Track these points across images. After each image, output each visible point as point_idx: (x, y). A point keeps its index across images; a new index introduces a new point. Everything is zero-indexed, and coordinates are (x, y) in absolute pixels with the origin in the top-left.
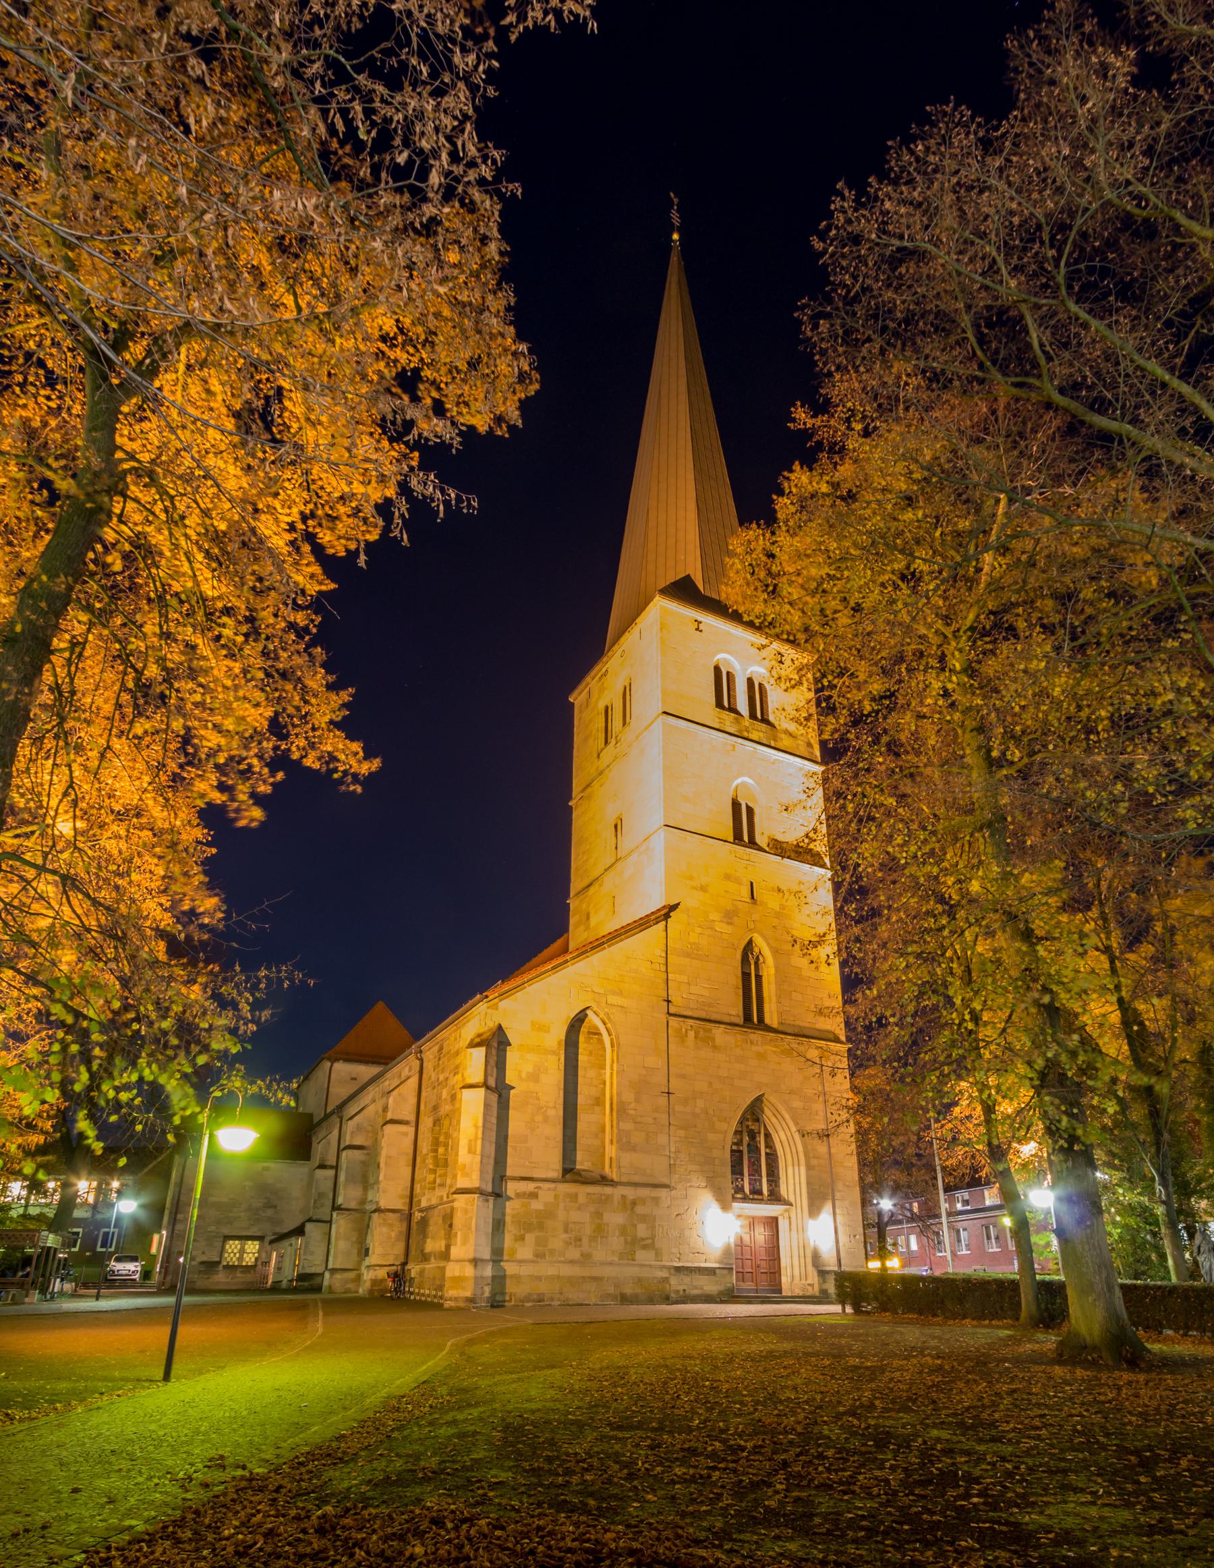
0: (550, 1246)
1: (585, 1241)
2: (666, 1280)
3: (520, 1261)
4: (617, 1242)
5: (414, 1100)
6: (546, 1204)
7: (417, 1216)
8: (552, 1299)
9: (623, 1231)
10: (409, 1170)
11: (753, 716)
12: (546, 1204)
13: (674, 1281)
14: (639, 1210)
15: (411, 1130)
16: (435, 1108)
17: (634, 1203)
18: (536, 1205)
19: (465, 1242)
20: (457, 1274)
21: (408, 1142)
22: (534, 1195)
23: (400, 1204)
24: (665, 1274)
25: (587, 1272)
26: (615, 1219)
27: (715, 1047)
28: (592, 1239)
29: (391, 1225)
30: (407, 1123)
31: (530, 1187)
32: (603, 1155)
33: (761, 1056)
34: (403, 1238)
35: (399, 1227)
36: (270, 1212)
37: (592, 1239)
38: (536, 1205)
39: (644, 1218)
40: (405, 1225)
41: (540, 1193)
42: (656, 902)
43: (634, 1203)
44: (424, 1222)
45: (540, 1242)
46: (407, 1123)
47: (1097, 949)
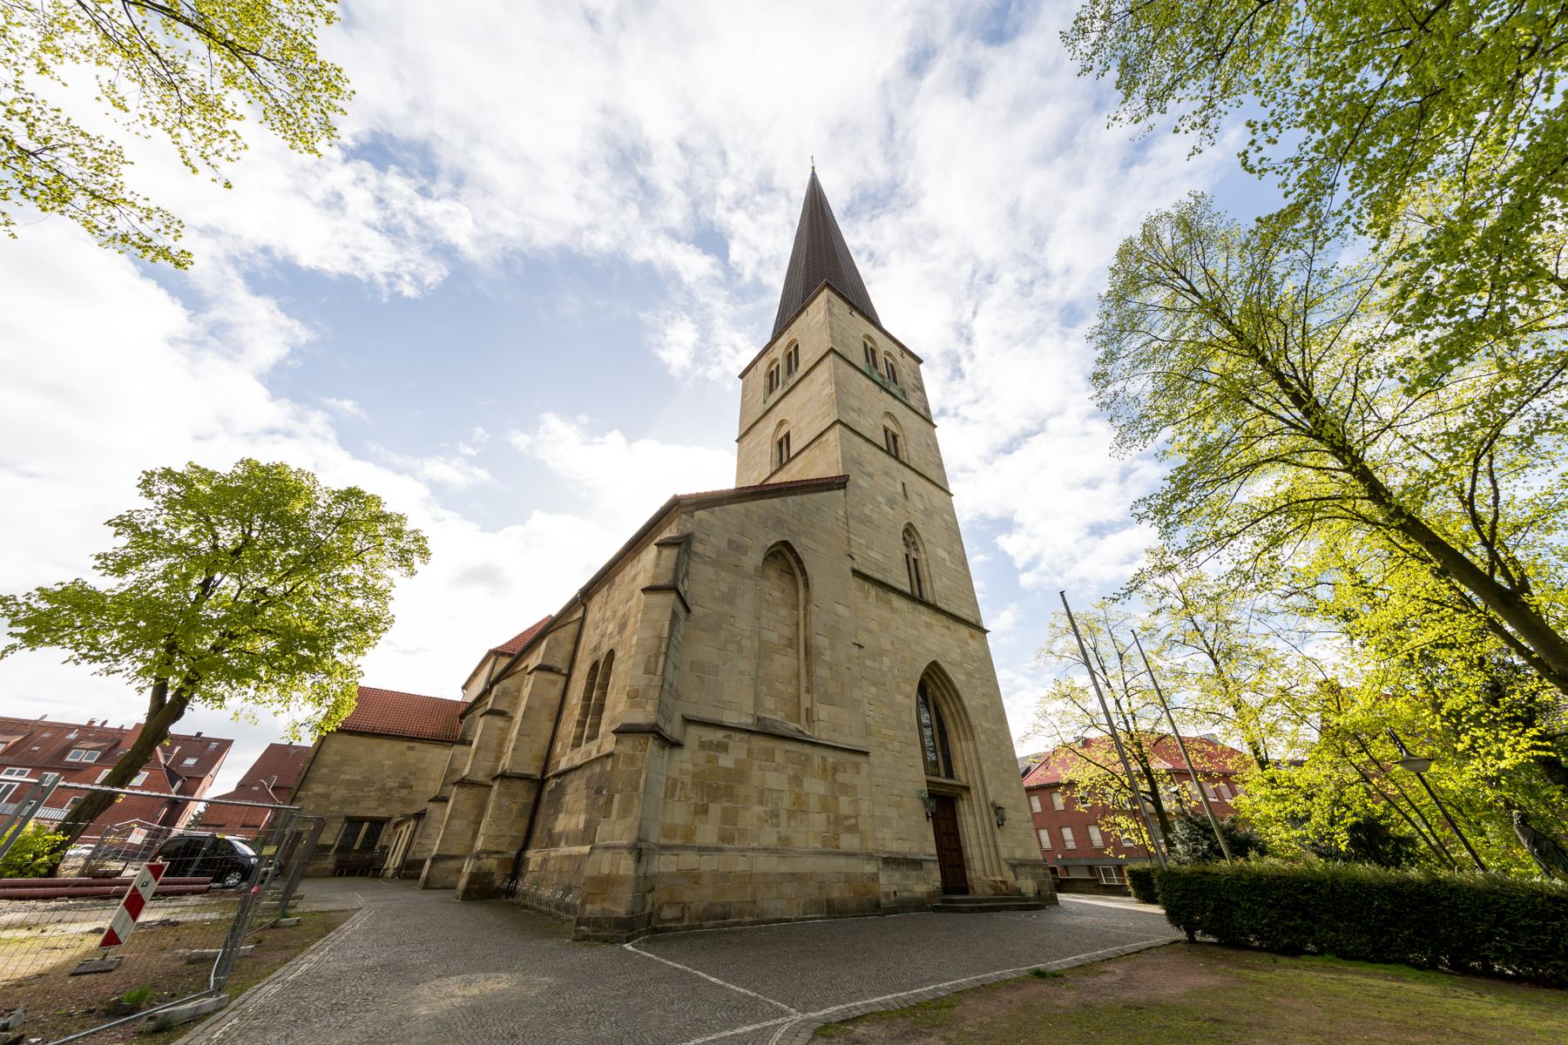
0: (741, 824)
1: (783, 816)
3: (702, 850)
4: (818, 821)
5: (570, 647)
6: (737, 762)
8: (741, 913)
10: (551, 725)
12: (737, 762)
13: (883, 879)
14: (841, 777)
15: (561, 681)
18: (726, 761)
19: (624, 813)
20: (605, 870)
21: (555, 692)
22: (722, 747)
23: (533, 769)
24: (870, 868)
25: (785, 867)
26: (815, 787)
27: (892, 609)
28: (791, 815)
29: (514, 796)
30: (558, 672)
31: (719, 735)
32: (798, 704)
33: (929, 626)
34: (528, 813)
35: (523, 794)
36: (404, 792)
37: (791, 815)
38: (726, 761)
40: (533, 796)
41: (732, 744)
42: (833, 472)
43: (835, 769)
44: (560, 790)
45: (729, 817)
46: (558, 672)
47: (1548, 99)
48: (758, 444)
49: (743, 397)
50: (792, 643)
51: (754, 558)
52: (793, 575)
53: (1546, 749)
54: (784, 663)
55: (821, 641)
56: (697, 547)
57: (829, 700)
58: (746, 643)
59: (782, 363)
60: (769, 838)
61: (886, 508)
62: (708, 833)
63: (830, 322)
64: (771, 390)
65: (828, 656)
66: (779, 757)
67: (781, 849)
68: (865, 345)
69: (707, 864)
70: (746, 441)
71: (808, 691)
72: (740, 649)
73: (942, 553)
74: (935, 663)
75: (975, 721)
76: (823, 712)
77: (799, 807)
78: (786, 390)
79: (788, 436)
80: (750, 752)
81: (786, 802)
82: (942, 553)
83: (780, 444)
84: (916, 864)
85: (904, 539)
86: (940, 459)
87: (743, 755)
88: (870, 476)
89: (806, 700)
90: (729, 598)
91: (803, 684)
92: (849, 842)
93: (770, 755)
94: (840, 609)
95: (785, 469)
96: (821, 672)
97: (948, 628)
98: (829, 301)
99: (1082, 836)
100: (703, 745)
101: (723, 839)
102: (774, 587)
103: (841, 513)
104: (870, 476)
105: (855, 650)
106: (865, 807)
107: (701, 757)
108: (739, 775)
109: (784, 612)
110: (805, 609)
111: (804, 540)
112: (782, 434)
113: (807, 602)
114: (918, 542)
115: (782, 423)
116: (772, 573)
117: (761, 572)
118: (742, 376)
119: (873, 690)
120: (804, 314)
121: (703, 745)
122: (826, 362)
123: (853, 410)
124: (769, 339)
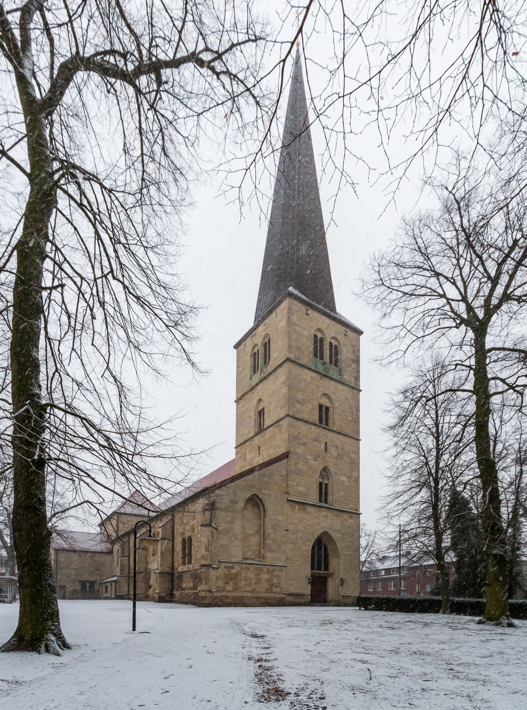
2: (285, 598)
3: (228, 591)
7: (177, 575)
9: (268, 581)
11: (331, 362)
12: (237, 571)
16: (183, 533)
17: (272, 571)
18: (233, 571)
22: (232, 568)
28: (256, 583)
31: (231, 565)
33: (326, 517)
38: (233, 571)
39: (276, 576)
42: (282, 450)
48: (248, 409)
49: (238, 367)
50: (258, 532)
51: (241, 504)
52: (258, 505)
53: (111, 588)
54: (255, 540)
55: (269, 531)
56: (217, 505)
57: (272, 551)
58: (239, 536)
59: (260, 347)
60: (249, 588)
61: (312, 462)
62: (229, 588)
63: (289, 333)
64: (255, 372)
65: (272, 536)
66: (251, 569)
67: (253, 591)
68: (315, 336)
69: (230, 594)
70: (242, 403)
71: (264, 548)
72: (237, 538)
73: (344, 478)
74: (325, 534)
75: (340, 551)
76: (269, 555)
77: (259, 581)
78: (263, 375)
79: (263, 409)
80: (241, 568)
81: (254, 580)
82: (344, 478)
83: (260, 413)
84: (301, 595)
85: (321, 474)
86: (358, 416)
87: (239, 569)
88: (305, 444)
89: (263, 552)
90: (232, 522)
91: (262, 547)
92: (275, 590)
93: (249, 569)
94: (280, 518)
95: (262, 434)
96: (269, 542)
97: (337, 516)
98: (290, 311)
99: (385, 588)
100: (226, 567)
101: (234, 589)
102: (250, 514)
103: (284, 472)
104: (305, 444)
105: (286, 532)
106: (283, 581)
107: (226, 570)
108: (238, 574)
109: (254, 522)
110: (264, 520)
111: (264, 491)
112: (260, 408)
113: (264, 517)
114: (330, 475)
115: (260, 400)
116: (249, 507)
117: (245, 508)
118: (236, 346)
119: (292, 546)
120: (274, 315)
121: (226, 567)
122: (285, 366)
123: (299, 402)
124: (251, 324)
